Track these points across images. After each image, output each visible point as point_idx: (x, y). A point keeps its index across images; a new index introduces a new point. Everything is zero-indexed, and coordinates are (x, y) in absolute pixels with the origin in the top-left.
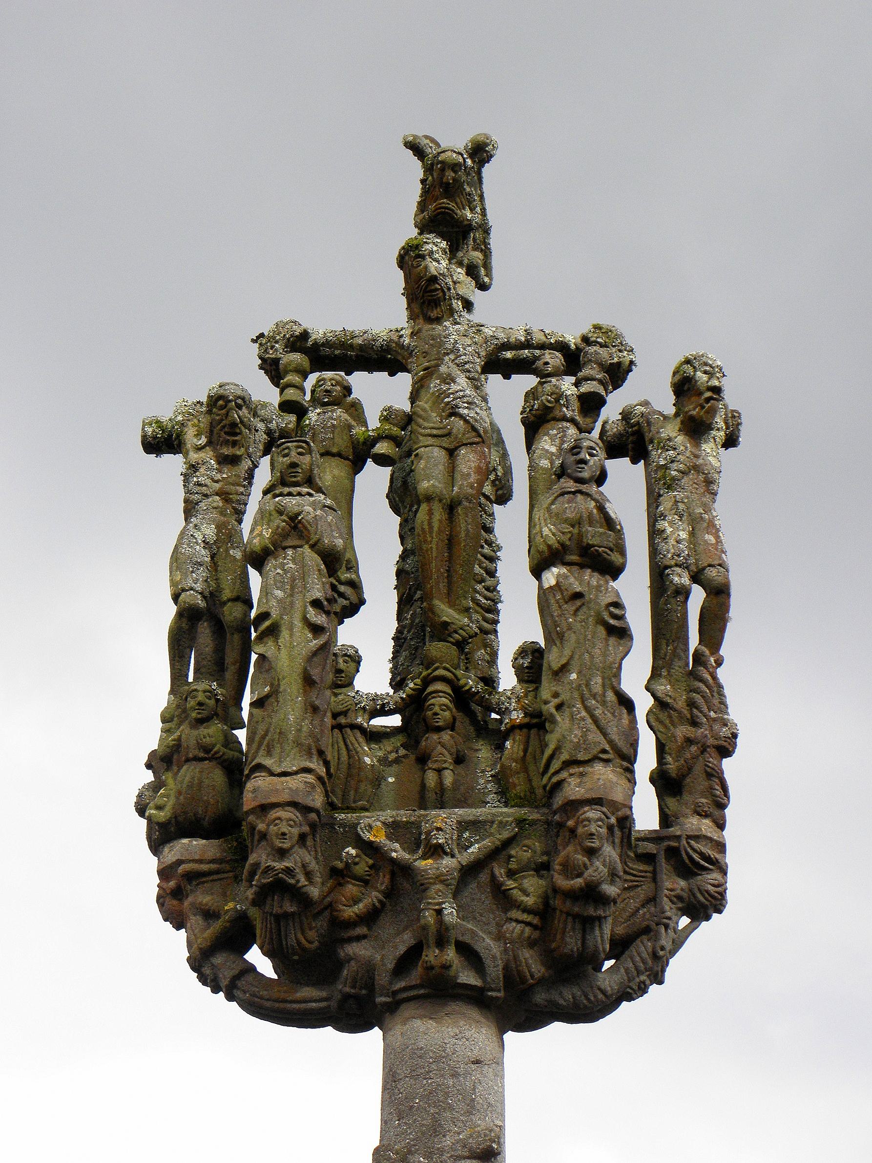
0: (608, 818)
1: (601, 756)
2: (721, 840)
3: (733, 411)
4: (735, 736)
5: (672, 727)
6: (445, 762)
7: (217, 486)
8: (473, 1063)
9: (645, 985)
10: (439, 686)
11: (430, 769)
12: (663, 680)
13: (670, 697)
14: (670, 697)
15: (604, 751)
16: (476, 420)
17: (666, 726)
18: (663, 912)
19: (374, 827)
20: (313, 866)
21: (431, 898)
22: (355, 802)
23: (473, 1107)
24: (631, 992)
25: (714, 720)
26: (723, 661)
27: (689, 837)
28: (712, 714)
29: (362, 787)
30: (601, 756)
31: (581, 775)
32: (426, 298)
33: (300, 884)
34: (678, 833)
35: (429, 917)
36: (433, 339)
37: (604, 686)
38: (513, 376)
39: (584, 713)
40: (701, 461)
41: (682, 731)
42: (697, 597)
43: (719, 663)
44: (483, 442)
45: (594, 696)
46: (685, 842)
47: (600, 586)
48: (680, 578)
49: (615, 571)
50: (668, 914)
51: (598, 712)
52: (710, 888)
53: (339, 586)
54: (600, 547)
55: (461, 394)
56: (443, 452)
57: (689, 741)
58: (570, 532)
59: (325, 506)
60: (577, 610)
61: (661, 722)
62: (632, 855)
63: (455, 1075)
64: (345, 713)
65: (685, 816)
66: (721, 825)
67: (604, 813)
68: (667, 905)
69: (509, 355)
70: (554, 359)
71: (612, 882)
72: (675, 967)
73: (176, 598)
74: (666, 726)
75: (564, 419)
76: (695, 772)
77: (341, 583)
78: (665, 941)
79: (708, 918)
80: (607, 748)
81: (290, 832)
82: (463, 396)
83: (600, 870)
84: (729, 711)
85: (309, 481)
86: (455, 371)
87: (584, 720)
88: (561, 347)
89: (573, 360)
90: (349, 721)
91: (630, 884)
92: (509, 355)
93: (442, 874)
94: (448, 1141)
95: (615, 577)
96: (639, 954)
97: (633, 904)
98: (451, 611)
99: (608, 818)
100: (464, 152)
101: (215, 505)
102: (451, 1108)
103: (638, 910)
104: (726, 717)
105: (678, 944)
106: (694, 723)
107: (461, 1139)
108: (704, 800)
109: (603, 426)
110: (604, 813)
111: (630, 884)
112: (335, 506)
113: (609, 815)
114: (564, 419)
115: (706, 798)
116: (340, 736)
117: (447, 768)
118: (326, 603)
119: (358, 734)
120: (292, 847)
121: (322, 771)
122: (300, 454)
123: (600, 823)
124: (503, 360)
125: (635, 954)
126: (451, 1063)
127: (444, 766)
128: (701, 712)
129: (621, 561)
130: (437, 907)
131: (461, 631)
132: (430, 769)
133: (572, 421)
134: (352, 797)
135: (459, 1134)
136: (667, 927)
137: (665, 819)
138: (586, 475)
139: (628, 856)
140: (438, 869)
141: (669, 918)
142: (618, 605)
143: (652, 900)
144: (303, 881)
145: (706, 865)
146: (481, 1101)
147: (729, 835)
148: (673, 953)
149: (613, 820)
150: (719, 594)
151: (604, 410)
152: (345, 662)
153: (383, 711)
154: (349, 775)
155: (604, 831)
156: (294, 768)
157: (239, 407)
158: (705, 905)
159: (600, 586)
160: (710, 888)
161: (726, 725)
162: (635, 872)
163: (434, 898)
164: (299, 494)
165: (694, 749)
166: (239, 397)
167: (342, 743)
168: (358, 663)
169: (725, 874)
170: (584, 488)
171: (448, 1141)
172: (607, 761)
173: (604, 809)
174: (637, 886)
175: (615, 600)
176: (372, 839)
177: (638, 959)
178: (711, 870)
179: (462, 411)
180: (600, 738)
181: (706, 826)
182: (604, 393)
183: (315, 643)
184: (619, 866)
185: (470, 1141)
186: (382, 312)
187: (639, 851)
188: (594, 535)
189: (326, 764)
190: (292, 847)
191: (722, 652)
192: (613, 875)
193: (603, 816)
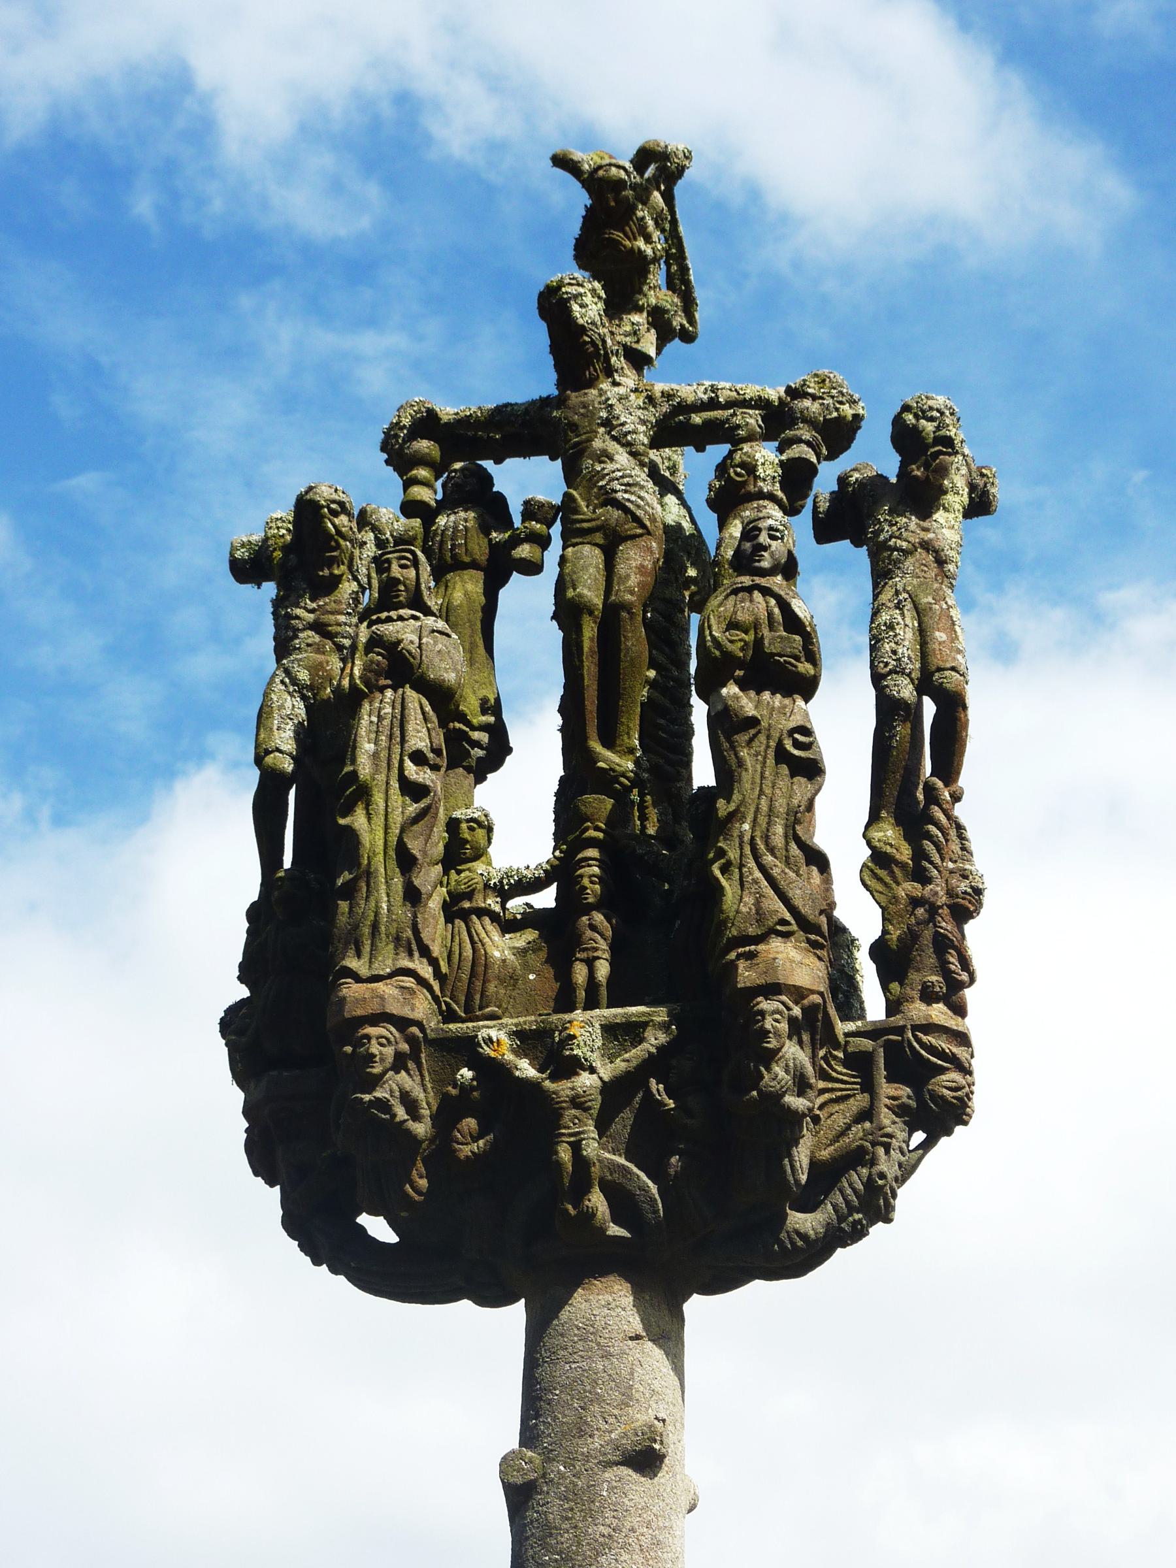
0: (789, 1009)
1: (779, 928)
2: (960, 1029)
3: (980, 469)
4: (978, 892)
5: (894, 885)
6: (596, 949)
7: (311, 617)
8: (631, 1338)
9: (862, 1225)
10: (593, 853)
11: (577, 959)
12: (884, 825)
13: (891, 845)
14: (891, 845)
15: (783, 922)
16: (638, 506)
17: (886, 884)
18: (881, 1129)
19: (496, 1036)
20: (418, 1093)
21: (565, 1128)
22: (481, 1008)
23: (630, 1397)
24: (843, 1234)
25: (951, 872)
26: (962, 793)
27: (915, 1028)
28: (951, 865)
29: (492, 987)
30: (779, 928)
31: (751, 956)
32: (576, 357)
33: (398, 1119)
34: (901, 1023)
35: (564, 1154)
36: (584, 407)
37: (786, 836)
38: (708, 447)
39: (758, 874)
40: (931, 535)
41: (907, 888)
42: (929, 708)
43: (956, 798)
44: (649, 533)
45: (772, 850)
46: (910, 1035)
47: (785, 707)
48: (905, 690)
49: (807, 688)
50: (889, 1130)
51: (775, 872)
52: (946, 1092)
53: (471, 733)
54: (781, 656)
55: (620, 474)
56: (597, 551)
57: (915, 902)
58: (740, 640)
59: (433, 631)
60: (751, 740)
61: (880, 879)
62: (841, 1055)
63: (607, 1356)
64: (469, 895)
65: (911, 1000)
66: (960, 1010)
67: (783, 1003)
68: (886, 1118)
69: (697, 419)
70: (753, 419)
71: (801, 1094)
72: (906, 1198)
73: (259, 761)
74: (886, 884)
75: (761, 495)
76: (929, 943)
77: (473, 728)
78: (887, 1165)
79: (949, 1133)
80: (788, 916)
81: (381, 1053)
82: (622, 477)
83: (780, 1077)
84: (974, 859)
85: (417, 603)
86: (613, 447)
87: (757, 883)
88: (761, 403)
89: (778, 419)
90: (474, 904)
91: (839, 1094)
92: (697, 419)
93: (578, 1096)
94: (597, 1443)
95: (808, 696)
96: (851, 1185)
97: (840, 1121)
98: (608, 754)
99: (789, 1009)
100: (628, 165)
101: (309, 641)
102: (599, 1399)
103: (848, 1127)
104: (967, 867)
105: (907, 1171)
106: (922, 877)
107: (611, 1440)
108: (934, 978)
109: (815, 502)
110: (783, 1003)
111: (839, 1094)
112: (449, 631)
113: (791, 1004)
114: (761, 495)
115: (938, 975)
116: (463, 925)
117: (599, 958)
118: (431, 755)
119: (487, 920)
120: (385, 1073)
121: (426, 971)
122: (403, 567)
123: (778, 1016)
124: (677, 427)
125: (846, 1185)
126: (602, 1341)
127: (595, 954)
128: (931, 863)
129: (812, 672)
130: (572, 1139)
131: (622, 779)
132: (577, 959)
133: (771, 497)
134: (478, 1002)
135: (611, 1432)
136: (887, 1148)
137: (893, 1007)
138: (765, 564)
139: (835, 1058)
140: (573, 1089)
141: (890, 1136)
142: (806, 731)
143: (867, 1114)
144: (401, 1113)
145: (940, 1062)
146: (641, 1389)
147: (972, 1024)
148: (902, 1180)
149: (797, 1011)
150: (952, 708)
151: (817, 480)
152: (471, 829)
153: (535, 885)
154: (473, 974)
155: (784, 1026)
156: (388, 970)
157: (335, 514)
158: (942, 1115)
159: (785, 707)
160: (946, 1092)
161: (965, 877)
162: (845, 1078)
163: (569, 1128)
164: (401, 618)
165: (920, 911)
166: (334, 502)
167: (465, 933)
168: (490, 830)
169: (970, 1073)
170: (763, 581)
171: (597, 1443)
172: (786, 935)
173: (784, 998)
174: (848, 1097)
175: (800, 723)
176: (493, 1054)
177: (849, 1191)
178: (948, 1069)
179: (619, 495)
180: (780, 906)
181: (938, 1013)
182: (814, 459)
183: (413, 808)
184: (810, 1070)
185: (624, 1442)
186: (529, 377)
187: (850, 1050)
188: (775, 640)
189: (434, 962)
190: (385, 1073)
191: (963, 781)
192: (802, 1086)
193: (781, 1007)
